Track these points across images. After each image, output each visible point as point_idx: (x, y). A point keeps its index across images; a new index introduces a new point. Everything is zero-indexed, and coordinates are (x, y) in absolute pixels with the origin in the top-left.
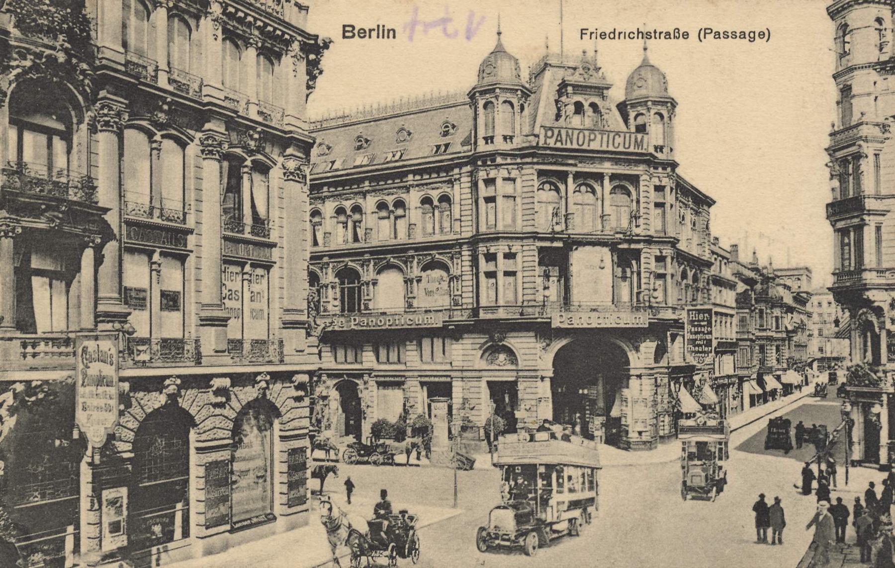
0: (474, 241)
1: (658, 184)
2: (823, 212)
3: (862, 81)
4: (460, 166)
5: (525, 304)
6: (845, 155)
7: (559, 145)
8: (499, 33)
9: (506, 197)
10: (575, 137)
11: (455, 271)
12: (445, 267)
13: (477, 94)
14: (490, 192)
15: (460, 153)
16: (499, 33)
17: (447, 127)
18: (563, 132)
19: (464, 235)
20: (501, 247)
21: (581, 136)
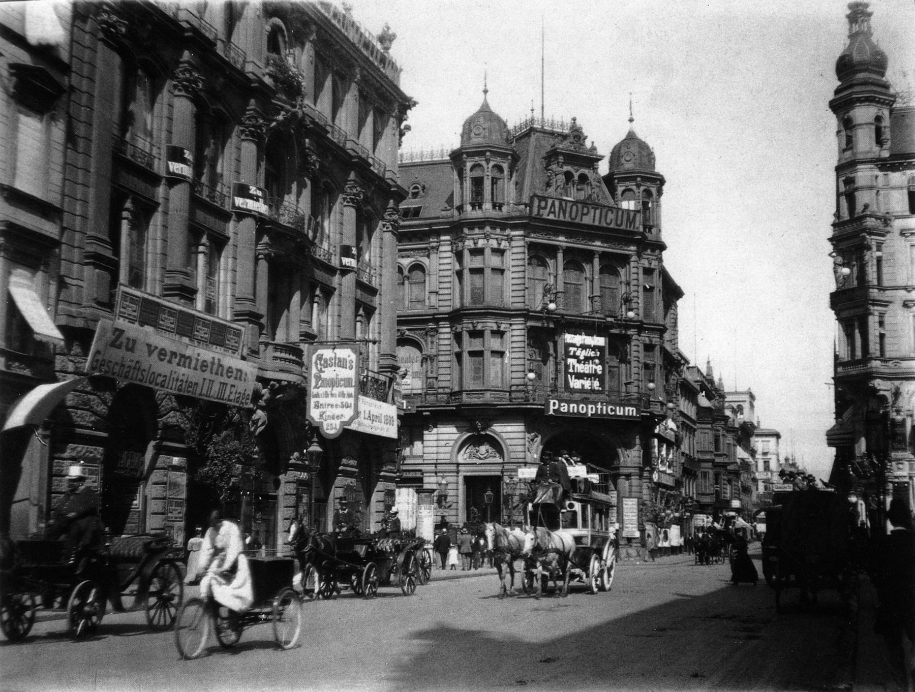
0: (455, 317)
1: (647, 265)
2: (827, 300)
3: (864, 175)
4: (438, 233)
5: (514, 388)
6: (853, 238)
7: (551, 217)
8: (486, 92)
9: (494, 270)
10: (568, 209)
11: (430, 350)
12: (417, 346)
13: (465, 156)
14: (477, 262)
15: (438, 218)
16: (486, 92)
17: (416, 188)
18: (557, 203)
19: (442, 310)
20: (489, 324)
21: (574, 207)
